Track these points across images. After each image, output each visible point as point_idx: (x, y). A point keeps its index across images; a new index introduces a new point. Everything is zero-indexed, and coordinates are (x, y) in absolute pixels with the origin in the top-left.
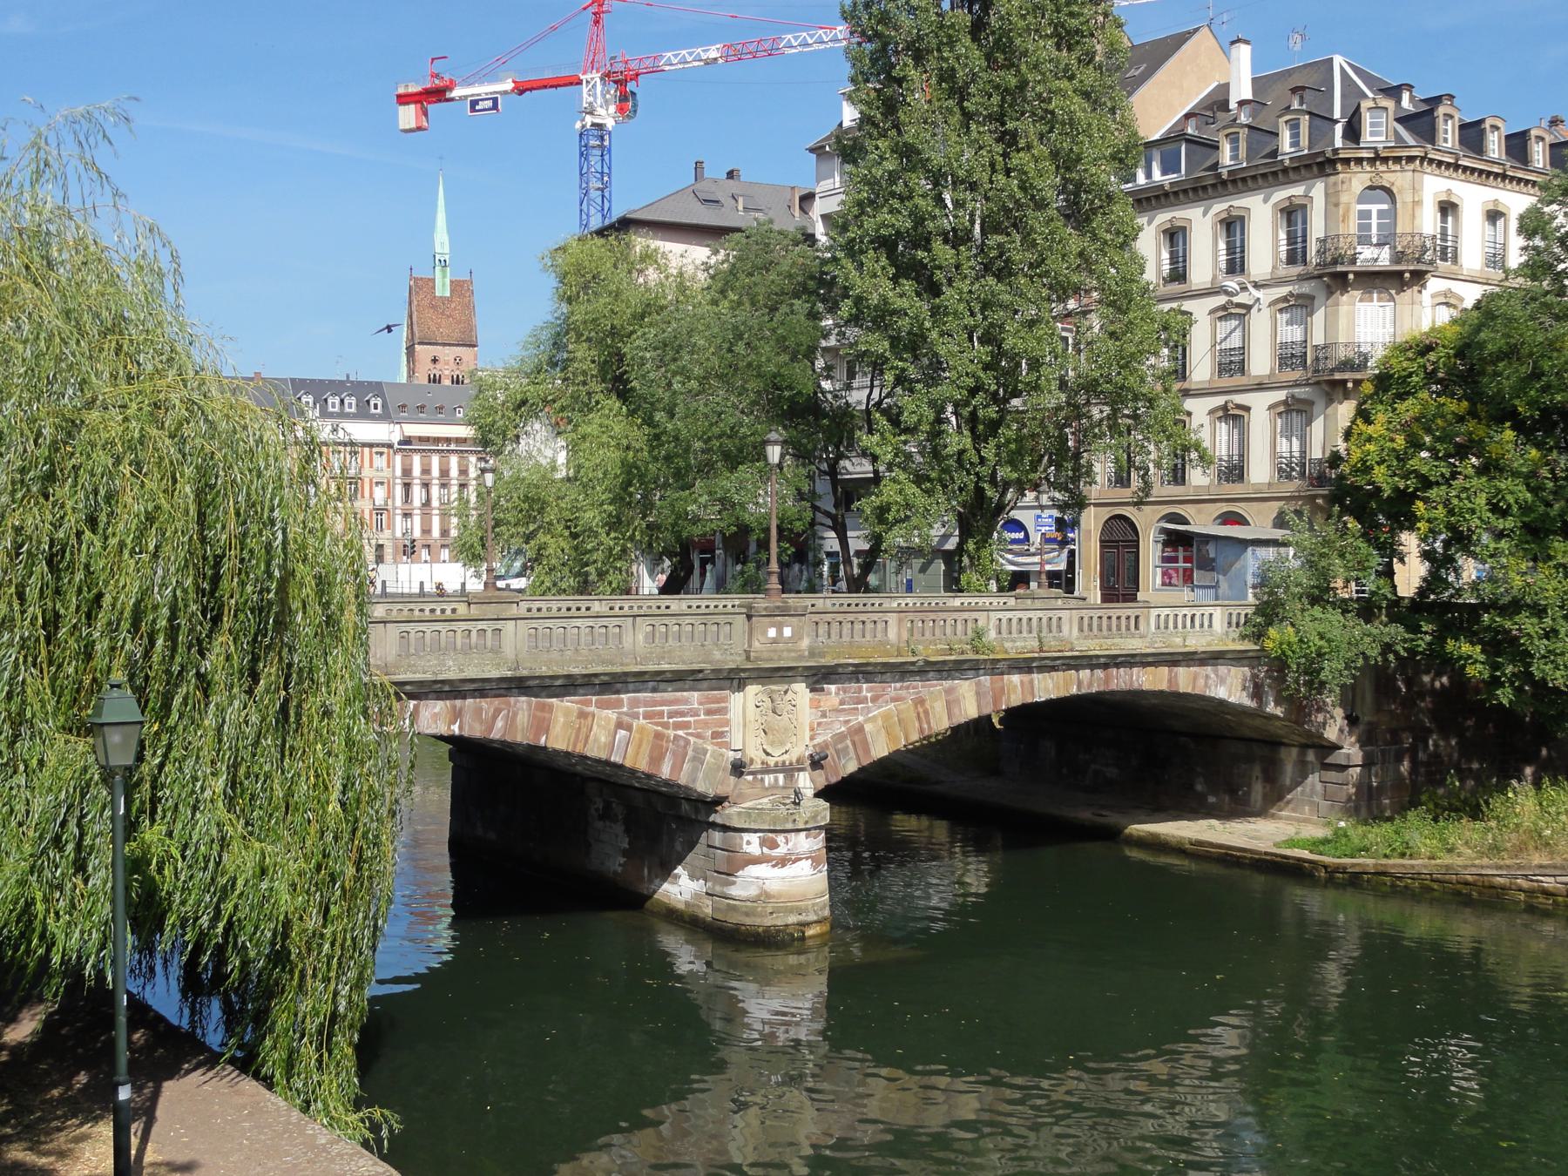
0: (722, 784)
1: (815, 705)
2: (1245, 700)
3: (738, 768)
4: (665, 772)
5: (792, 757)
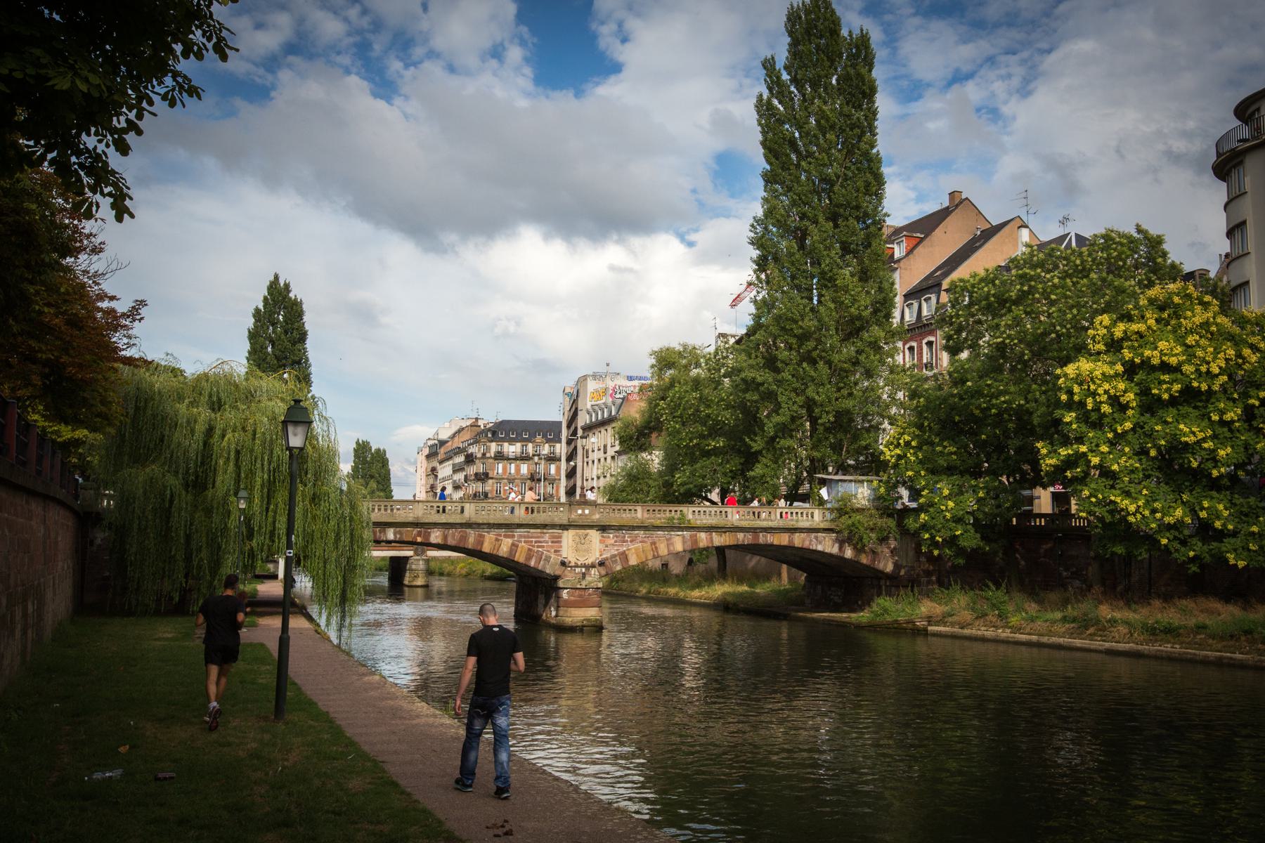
0: (558, 571)
1: (601, 542)
2: (835, 550)
3: (563, 564)
4: (532, 564)
5: (589, 562)
